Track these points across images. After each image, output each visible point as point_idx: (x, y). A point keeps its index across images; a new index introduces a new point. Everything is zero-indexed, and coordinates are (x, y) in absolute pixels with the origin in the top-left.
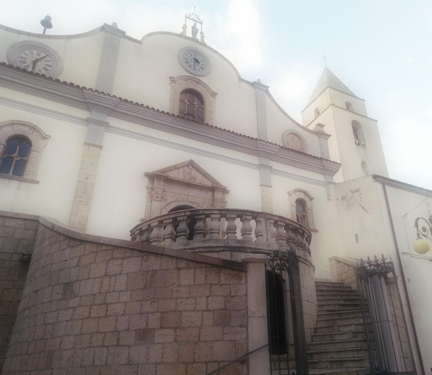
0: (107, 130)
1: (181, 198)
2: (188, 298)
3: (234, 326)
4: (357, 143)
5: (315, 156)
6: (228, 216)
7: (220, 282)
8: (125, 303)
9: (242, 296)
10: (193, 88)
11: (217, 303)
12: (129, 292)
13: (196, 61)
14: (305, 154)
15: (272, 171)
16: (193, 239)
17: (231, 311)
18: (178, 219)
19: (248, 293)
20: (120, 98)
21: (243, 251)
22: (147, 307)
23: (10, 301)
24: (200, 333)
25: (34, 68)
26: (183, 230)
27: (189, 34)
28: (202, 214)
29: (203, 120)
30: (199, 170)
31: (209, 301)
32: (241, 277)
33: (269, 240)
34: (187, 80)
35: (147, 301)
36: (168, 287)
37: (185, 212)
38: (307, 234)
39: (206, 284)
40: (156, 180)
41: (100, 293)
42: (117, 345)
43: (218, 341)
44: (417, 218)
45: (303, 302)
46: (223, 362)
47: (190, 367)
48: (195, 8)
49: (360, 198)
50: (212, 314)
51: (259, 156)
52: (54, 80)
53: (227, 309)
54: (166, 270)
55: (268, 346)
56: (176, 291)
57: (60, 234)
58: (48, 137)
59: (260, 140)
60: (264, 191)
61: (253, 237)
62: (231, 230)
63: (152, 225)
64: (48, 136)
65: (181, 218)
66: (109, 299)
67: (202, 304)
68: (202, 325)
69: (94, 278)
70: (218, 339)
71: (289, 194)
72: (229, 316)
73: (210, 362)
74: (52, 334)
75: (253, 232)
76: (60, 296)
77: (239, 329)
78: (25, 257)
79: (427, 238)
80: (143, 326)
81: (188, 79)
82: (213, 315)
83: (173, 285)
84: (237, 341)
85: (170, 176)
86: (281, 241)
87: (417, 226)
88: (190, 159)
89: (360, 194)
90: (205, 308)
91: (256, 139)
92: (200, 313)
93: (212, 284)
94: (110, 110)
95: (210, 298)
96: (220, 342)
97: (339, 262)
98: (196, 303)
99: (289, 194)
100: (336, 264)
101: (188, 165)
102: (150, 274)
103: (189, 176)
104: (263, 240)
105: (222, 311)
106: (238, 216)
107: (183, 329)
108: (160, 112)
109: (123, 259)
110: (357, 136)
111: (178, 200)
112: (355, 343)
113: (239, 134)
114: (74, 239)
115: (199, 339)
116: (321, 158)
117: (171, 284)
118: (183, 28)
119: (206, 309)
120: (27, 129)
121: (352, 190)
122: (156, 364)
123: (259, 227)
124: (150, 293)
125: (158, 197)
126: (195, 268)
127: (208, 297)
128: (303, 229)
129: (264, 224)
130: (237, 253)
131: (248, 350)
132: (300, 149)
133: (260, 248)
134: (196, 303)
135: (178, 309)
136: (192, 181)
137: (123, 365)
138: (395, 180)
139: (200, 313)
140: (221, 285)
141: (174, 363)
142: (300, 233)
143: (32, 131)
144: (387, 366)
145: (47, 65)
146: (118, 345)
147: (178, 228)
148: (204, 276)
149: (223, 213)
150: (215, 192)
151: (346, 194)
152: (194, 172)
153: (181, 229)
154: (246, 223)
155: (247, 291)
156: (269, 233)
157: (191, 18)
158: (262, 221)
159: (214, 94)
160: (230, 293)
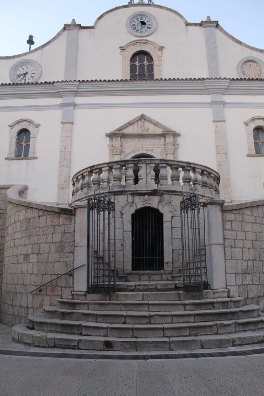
1: (136, 149)
3: (66, 253)
9: (72, 232)
10: (141, 50)
11: (57, 238)
12: (21, 232)
17: (65, 243)
19: (76, 230)
21: (124, 194)
30: (150, 121)
31: (53, 236)
32: (72, 219)
33: (148, 182)
34: (136, 44)
43: (57, 262)
46: (60, 274)
47: (43, 277)
50: (54, 245)
51: (209, 94)
54: (34, 217)
56: (38, 231)
58: (39, 125)
64: (38, 124)
68: (49, 252)
70: (57, 261)
71: (246, 124)
73: (53, 274)
77: (69, 254)
81: (136, 43)
83: (37, 227)
90: (51, 241)
94: (75, 92)
95: (54, 235)
96: (58, 263)
99: (246, 124)
101: (140, 119)
103: (142, 128)
105: (60, 243)
107: (41, 254)
108: (111, 82)
111: (135, 150)
113: (180, 79)
115: (48, 261)
119: (52, 242)
120: (26, 123)
125: (117, 152)
127: (53, 234)
129: (145, 168)
130: (119, 196)
131: (73, 268)
132: (259, 75)
133: (139, 189)
136: (146, 133)
141: (37, 274)
143: (29, 124)
146: (18, 263)
148: (51, 220)
150: (166, 137)
155: (75, 229)
158: (143, 167)
159: (162, 48)
160: (65, 230)
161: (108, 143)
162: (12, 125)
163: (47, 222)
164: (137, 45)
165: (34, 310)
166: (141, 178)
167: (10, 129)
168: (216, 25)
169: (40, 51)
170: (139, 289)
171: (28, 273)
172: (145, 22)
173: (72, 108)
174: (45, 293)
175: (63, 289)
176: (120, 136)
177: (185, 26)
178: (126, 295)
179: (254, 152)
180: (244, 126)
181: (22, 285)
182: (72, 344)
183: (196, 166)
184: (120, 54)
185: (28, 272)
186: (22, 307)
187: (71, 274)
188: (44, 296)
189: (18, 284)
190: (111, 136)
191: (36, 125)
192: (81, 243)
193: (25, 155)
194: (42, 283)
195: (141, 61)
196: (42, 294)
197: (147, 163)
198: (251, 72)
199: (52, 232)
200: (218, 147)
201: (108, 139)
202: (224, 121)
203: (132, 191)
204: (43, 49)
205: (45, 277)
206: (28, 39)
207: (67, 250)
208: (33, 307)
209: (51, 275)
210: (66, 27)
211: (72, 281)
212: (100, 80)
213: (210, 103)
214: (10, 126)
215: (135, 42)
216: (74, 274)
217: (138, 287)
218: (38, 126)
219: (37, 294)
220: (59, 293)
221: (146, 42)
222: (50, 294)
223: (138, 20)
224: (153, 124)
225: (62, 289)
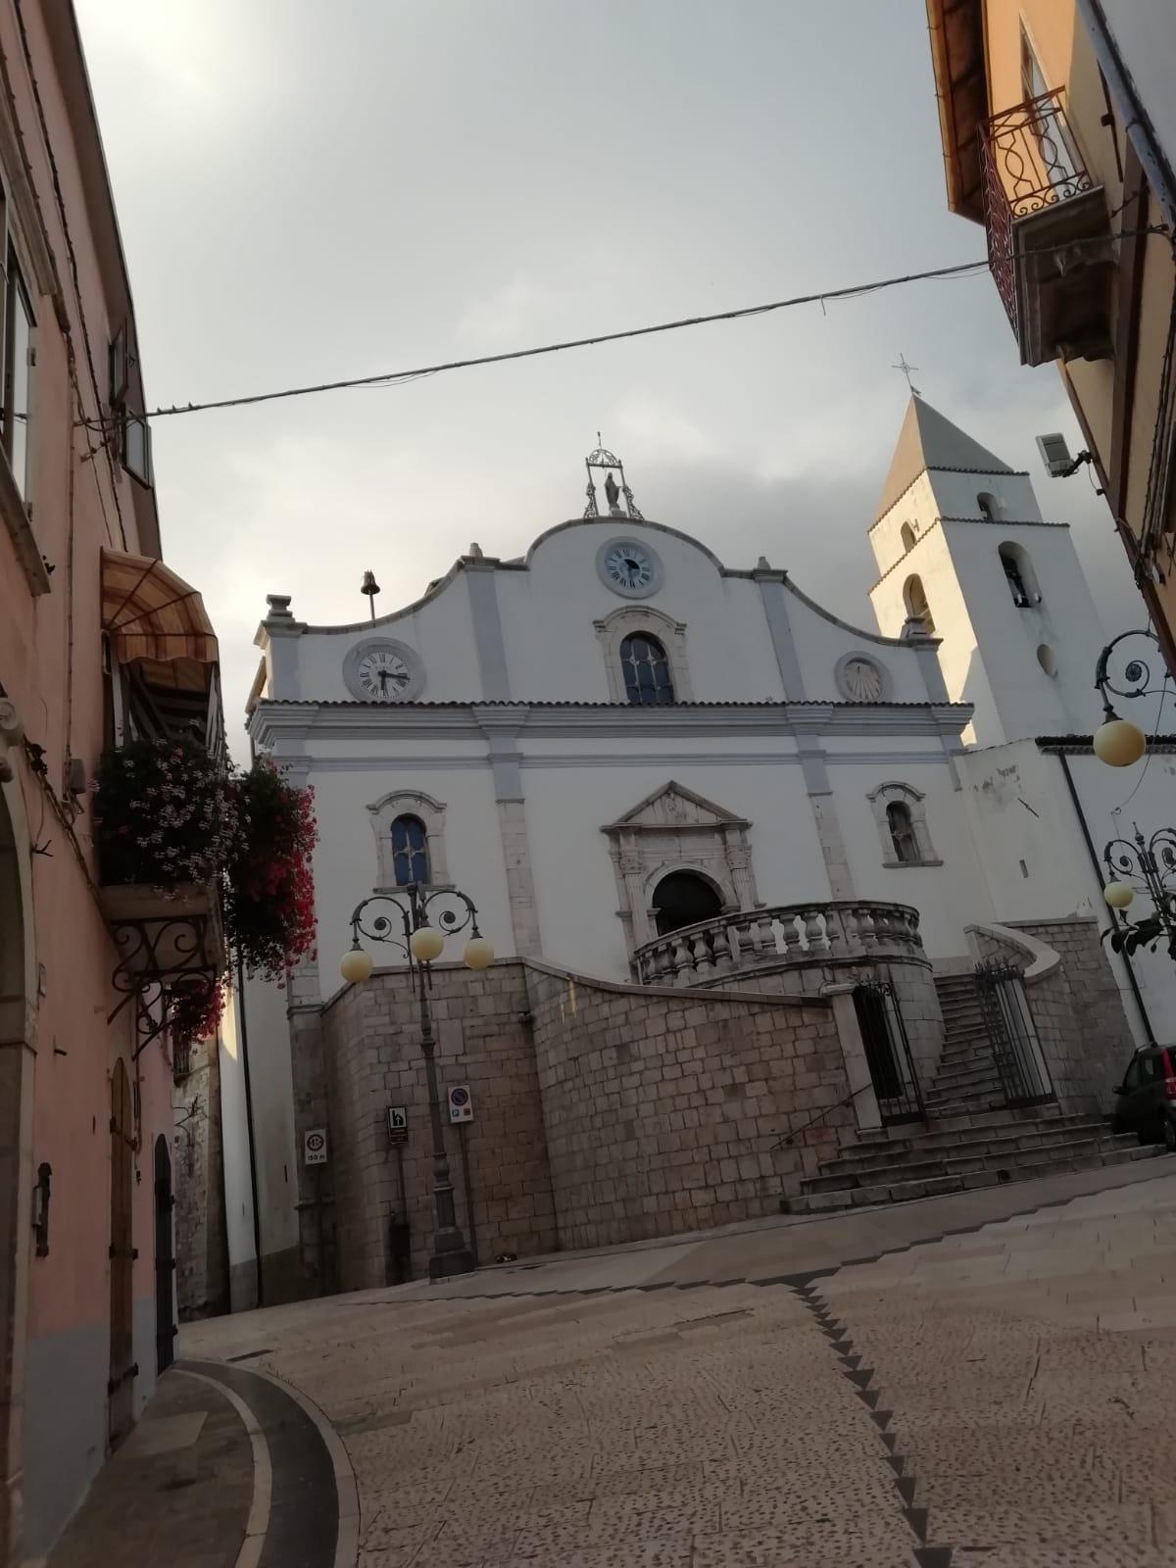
0: (522, 766)
4: (1020, 601)
7: (803, 1022)
8: (702, 1060)
10: (655, 633)
11: (806, 1047)
13: (632, 565)
14: (890, 705)
24: (794, 1081)
27: (604, 509)
28: (745, 921)
29: (669, 689)
30: (687, 796)
37: (719, 921)
39: (788, 1027)
48: (599, 434)
54: (739, 1018)
55: (872, 1087)
59: (792, 702)
61: (826, 942)
63: (673, 944)
65: (716, 931)
66: (683, 1056)
67: (789, 1050)
68: (794, 1073)
72: (825, 1058)
75: (824, 935)
77: (836, 1072)
86: (868, 940)
88: (669, 781)
89: (1018, 778)
90: (794, 1055)
92: (789, 1061)
95: (797, 1043)
97: (983, 935)
98: (782, 1051)
102: (721, 1024)
104: (840, 943)
107: (775, 1079)
111: (666, 862)
114: (610, 992)
118: (588, 494)
120: (411, 801)
121: (1001, 769)
122: (756, 1118)
123: (831, 924)
125: (633, 868)
127: (794, 1042)
128: (900, 909)
131: (850, 1092)
133: (839, 956)
134: (782, 1051)
136: (683, 824)
144: (1031, 1089)
146: (707, 1104)
148: (784, 1019)
152: (682, 805)
154: (811, 922)
156: (848, 930)
157: (598, 463)
161: (609, 848)
168: (782, 577)
169: (410, 618)
172: (637, 561)
173: (516, 764)
174: (802, 1144)
177: (719, 576)
179: (895, 857)
180: (868, 802)
182: (954, 1185)
183: (905, 910)
184: (596, 637)
187: (849, 1103)
190: (614, 832)
194: (790, 1128)
195: (642, 657)
200: (826, 851)
201: (606, 838)
202: (830, 794)
203: (829, 960)
206: (362, 583)
209: (808, 1110)
210: (462, 565)
211: (852, 1113)
213: (797, 756)
215: (624, 611)
221: (647, 612)
222: (814, 1142)
223: (620, 557)
224: (692, 802)
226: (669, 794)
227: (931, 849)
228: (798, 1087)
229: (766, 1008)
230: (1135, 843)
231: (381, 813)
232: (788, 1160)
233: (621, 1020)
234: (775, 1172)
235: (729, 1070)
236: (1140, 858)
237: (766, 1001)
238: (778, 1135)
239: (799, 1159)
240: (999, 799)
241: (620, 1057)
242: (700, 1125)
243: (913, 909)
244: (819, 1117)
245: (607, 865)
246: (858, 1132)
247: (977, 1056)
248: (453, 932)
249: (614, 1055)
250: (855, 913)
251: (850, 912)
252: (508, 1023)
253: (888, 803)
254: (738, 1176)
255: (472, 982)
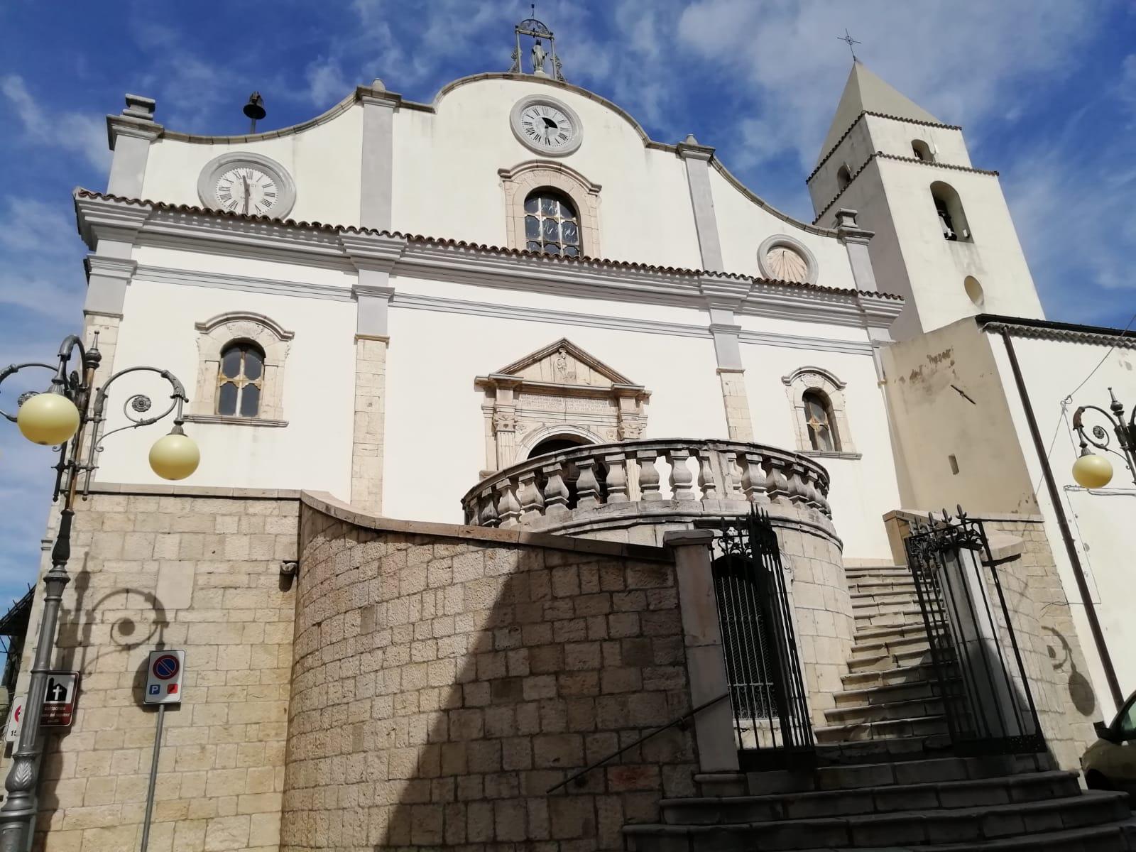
2: (573, 619)
4: (950, 235)
5: (837, 289)
6: (640, 455)
7: (626, 586)
11: (625, 625)
14: (814, 288)
15: (741, 336)
16: (576, 507)
17: (654, 639)
18: (545, 470)
20: (409, 236)
22: (504, 641)
23: (279, 645)
24: (600, 679)
25: (246, 205)
26: (556, 491)
35: (501, 628)
36: (534, 602)
37: (556, 456)
38: (814, 471)
39: (601, 591)
40: (498, 391)
41: (421, 620)
42: (461, 708)
43: (634, 692)
44: (1080, 408)
45: (1081, 601)
47: (589, 739)
49: (954, 372)
50: (618, 646)
52: (284, 222)
53: (645, 634)
54: (529, 571)
57: (341, 522)
60: (727, 384)
61: (696, 491)
62: (649, 484)
64: (290, 333)
65: (550, 469)
66: (440, 629)
67: (598, 629)
69: (408, 595)
70: (634, 689)
71: (786, 382)
73: (624, 729)
74: (355, 695)
75: (695, 483)
76: (359, 629)
77: (670, 670)
78: (288, 564)
79: (1107, 450)
80: (501, 672)
81: (537, 167)
82: (621, 646)
84: (669, 691)
85: (525, 379)
87: (1078, 425)
89: (952, 363)
91: (698, 272)
92: (596, 646)
93: (613, 592)
94: (393, 264)
98: (587, 628)
99: (786, 382)
100: (900, 527)
105: (637, 640)
106: (660, 453)
107: (571, 674)
109: (452, 557)
110: (950, 218)
111: (547, 425)
112: (929, 687)
116: (853, 290)
117: (540, 596)
119: (607, 638)
120: (252, 325)
121: (933, 356)
122: (532, 736)
124: (505, 614)
125: (506, 426)
126: (578, 565)
127: (607, 615)
128: (804, 463)
131: (690, 706)
134: (587, 628)
135: (558, 640)
136: (570, 384)
137: (476, 740)
138: (1037, 320)
139: (597, 646)
140: (630, 592)
141: (562, 733)
142: (798, 473)
145: (267, 194)
146: (463, 707)
147: (546, 488)
148: (596, 578)
149: (629, 449)
151: (921, 367)
153: (551, 488)
155: (679, 599)
156: (728, 479)
160: (648, 605)
162: (207, 326)
163: (584, 583)
164: (540, 173)
165: (559, 846)
166: (712, 484)
167: (200, 335)
170: (850, 757)
171: (520, 733)
174: (601, 789)
175: (666, 769)
176: (514, 386)
178: (857, 770)
181: (495, 772)
185: (518, 729)
186: (502, 843)
188: (598, 798)
189: (469, 774)
190: (490, 386)
191: (282, 332)
192: (704, 636)
193: (243, 412)
194: (585, 758)
196: (589, 794)
197: (720, 451)
198: (786, 268)
199: (606, 609)
202: (742, 372)
204: (297, 136)
205: (594, 739)
207: (661, 657)
208: (556, 837)
209: (617, 731)
211: (690, 743)
212: (463, 244)
214: (199, 327)
216: (694, 725)
217: (848, 753)
218: (286, 337)
219: (567, 794)
220: (655, 784)
221: (560, 169)
222: (621, 788)
223: (538, 115)
225: (661, 771)
226: (560, 353)
227: (850, 441)
228: (605, 690)
229: (572, 559)
230: (1111, 413)
231: (211, 334)
232: (574, 814)
233: (371, 570)
234: (550, 833)
235: (502, 654)
236: (1117, 430)
237: (571, 547)
238: (563, 769)
239: (592, 816)
240: (929, 390)
241: (364, 625)
242: (449, 741)
243: (823, 469)
244: (616, 754)
245: (481, 424)
246: (698, 777)
247: (899, 666)
248: (142, 423)
249: (358, 621)
250: (742, 460)
251: (734, 456)
252: (266, 572)
253: (805, 389)
254: (490, 833)
255: (223, 515)
